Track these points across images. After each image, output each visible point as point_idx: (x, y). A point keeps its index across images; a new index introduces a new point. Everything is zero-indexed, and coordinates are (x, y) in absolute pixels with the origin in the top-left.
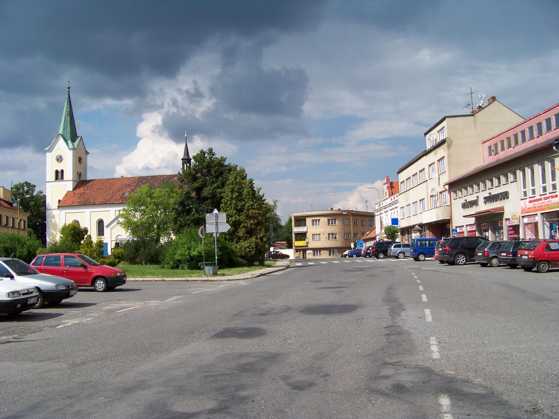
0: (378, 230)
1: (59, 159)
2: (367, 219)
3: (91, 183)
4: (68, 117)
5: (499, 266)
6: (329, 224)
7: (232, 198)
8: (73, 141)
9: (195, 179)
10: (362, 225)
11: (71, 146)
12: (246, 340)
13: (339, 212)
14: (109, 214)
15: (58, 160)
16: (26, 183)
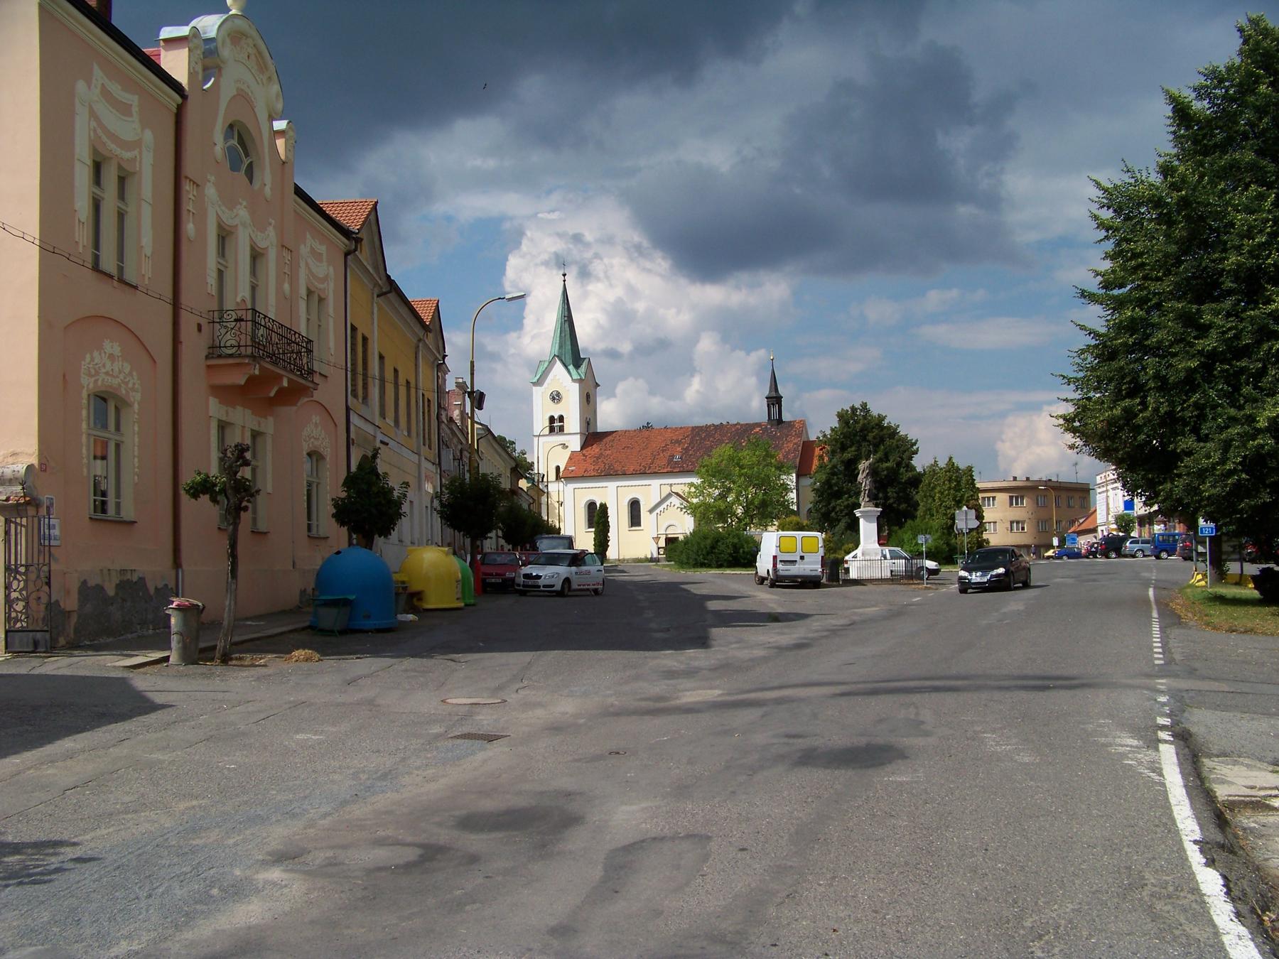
0: (1100, 517)
1: (556, 397)
2: (1077, 496)
3: (610, 438)
6: (1011, 504)
7: (950, 488)
8: (577, 366)
9: (844, 448)
10: (1069, 506)
11: (576, 376)
13: (1028, 484)
14: (650, 490)
15: (553, 399)
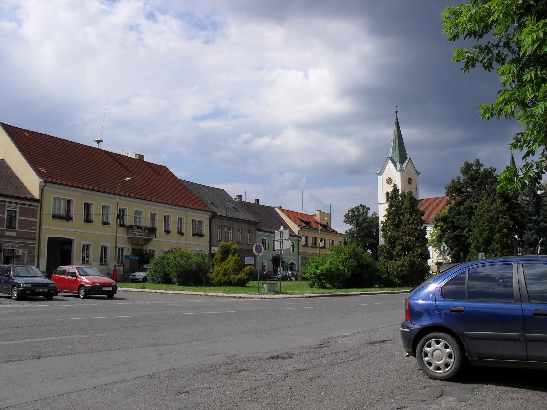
4: (397, 140)
5: (116, 247)
8: (402, 162)
12: (498, 387)
16: (361, 206)
